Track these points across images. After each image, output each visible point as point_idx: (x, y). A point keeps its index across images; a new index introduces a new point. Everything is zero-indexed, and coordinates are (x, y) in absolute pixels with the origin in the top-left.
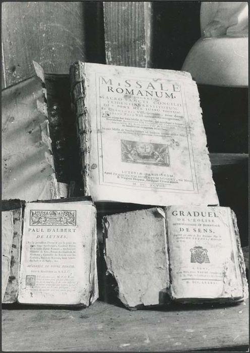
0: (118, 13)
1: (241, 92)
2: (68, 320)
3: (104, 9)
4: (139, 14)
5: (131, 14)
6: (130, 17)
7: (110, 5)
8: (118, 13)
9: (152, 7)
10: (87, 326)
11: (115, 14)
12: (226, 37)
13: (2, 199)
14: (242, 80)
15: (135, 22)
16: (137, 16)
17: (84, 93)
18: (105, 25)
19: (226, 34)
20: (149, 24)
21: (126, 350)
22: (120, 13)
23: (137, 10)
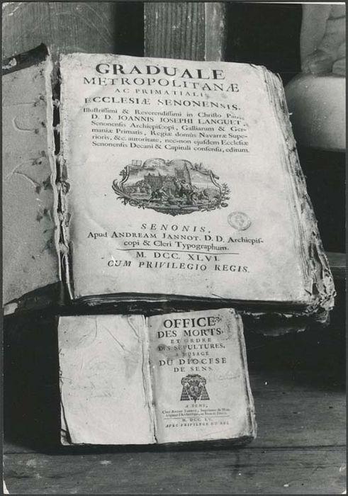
0: (166, 34)
1: (339, 155)
2: (31, 480)
3: (145, 28)
4: (197, 37)
5: (186, 36)
6: (183, 41)
7: (154, 23)
8: (166, 34)
9: (225, 26)
10: (55, 488)
11: (161, 35)
12: (331, 75)
13: (60, 318)
14: (341, 144)
15: (191, 47)
16: (194, 39)
17: (71, 152)
18: (145, 51)
19: (331, 71)
20: (220, 52)
21: (326, 492)
22: (169, 35)
23: (194, 31)
